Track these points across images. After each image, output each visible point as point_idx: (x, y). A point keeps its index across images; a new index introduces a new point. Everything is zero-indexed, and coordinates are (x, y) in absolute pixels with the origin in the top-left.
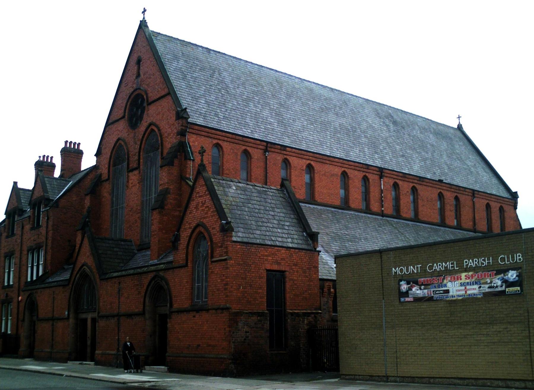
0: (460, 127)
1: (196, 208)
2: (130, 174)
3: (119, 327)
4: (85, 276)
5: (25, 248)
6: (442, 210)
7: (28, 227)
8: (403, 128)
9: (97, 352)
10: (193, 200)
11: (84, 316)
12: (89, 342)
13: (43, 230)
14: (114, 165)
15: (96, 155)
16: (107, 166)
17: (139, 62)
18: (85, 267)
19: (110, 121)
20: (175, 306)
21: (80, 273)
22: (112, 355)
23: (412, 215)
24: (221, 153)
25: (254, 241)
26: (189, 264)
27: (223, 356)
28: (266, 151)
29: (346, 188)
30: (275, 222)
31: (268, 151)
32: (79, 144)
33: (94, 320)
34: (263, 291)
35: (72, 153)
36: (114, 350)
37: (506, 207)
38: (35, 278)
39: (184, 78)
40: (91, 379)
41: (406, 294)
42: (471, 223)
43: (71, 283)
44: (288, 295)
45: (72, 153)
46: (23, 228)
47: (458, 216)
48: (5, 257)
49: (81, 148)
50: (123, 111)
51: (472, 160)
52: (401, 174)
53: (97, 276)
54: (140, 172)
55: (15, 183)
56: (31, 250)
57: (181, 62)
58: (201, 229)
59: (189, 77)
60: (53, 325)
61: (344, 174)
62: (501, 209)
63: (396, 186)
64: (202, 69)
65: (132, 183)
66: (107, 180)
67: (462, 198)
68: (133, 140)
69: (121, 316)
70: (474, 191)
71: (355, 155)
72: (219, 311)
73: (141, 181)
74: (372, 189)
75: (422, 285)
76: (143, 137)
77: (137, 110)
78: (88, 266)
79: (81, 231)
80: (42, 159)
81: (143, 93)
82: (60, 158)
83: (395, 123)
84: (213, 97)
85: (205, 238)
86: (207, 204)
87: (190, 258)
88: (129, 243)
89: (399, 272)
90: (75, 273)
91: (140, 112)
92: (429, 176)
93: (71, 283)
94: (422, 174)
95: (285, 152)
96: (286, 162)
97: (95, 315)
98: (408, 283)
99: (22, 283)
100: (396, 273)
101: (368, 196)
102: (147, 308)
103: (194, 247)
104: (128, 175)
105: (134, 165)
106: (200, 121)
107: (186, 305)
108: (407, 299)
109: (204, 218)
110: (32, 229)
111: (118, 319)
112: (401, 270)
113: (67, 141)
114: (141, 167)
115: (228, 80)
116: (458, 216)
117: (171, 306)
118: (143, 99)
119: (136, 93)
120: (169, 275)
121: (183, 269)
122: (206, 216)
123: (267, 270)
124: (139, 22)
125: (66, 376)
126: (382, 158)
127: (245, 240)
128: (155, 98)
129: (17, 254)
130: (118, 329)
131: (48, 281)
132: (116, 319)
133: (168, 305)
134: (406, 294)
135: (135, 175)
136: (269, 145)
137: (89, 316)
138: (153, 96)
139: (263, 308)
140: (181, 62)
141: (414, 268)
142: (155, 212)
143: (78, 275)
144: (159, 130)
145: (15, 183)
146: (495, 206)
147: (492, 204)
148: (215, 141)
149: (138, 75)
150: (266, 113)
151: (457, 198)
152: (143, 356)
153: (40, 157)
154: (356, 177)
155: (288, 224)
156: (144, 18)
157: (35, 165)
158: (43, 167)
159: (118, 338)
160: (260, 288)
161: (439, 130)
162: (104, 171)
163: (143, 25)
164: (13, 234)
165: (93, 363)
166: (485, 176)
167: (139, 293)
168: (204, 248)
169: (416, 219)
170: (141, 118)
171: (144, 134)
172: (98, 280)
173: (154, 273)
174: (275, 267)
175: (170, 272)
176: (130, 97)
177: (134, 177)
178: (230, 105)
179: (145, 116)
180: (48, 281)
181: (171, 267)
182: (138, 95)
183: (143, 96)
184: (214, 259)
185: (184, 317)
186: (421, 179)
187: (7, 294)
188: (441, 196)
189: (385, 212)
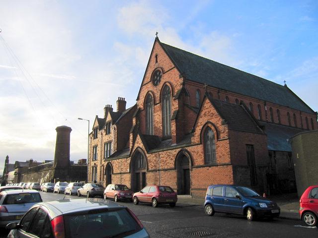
0: (286, 85)
7: (104, 134)
11: (138, 172)
15: (137, 100)
17: (156, 56)
19: (145, 83)
35: (122, 103)
42: (301, 126)
45: (122, 103)
48: (93, 148)
49: (125, 100)
55: (97, 116)
63: (271, 109)
68: (157, 91)
70: (301, 111)
81: (160, 70)
83: (262, 83)
85: (211, 129)
87: (202, 140)
91: (158, 78)
103: (204, 134)
107: (202, 164)
118: (160, 72)
123: (247, 145)
136: (220, 90)
139: (246, 164)
145: (97, 116)
148: (197, 88)
149: (157, 62)
151: (278, 111)
158: (108, 109)
162: (141, 106)
163: (157, 40)
174: (249, 143)
178: (199, 73)
179: (162, 79)
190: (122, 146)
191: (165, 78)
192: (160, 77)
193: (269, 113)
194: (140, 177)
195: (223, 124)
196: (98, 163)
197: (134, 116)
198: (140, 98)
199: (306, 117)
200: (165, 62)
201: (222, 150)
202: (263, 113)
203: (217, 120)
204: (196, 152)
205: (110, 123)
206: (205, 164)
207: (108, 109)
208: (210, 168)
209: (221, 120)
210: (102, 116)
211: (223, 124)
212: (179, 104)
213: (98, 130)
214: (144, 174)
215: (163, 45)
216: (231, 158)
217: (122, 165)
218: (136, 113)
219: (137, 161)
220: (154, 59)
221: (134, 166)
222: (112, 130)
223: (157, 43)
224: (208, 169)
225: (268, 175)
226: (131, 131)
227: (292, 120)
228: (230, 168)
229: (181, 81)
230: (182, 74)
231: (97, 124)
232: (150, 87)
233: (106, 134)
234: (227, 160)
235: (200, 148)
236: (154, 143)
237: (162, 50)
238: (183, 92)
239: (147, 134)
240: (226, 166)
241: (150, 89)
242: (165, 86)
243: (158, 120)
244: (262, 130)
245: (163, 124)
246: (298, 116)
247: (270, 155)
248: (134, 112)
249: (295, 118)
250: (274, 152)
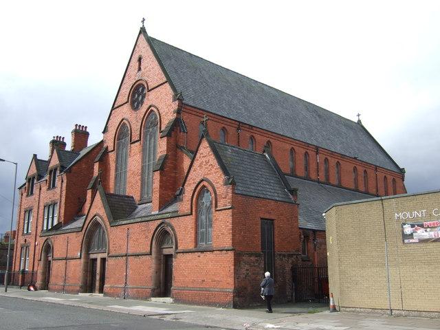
0: (359, 121)
1: (200, 166)
2: (132, 145)
4: (96, 225)
5: (42, 205)
6: (356, 180)
7: (25, 194)
8: (325, 120)
9: (105, 286)
10: (198, 160)
11: (93, 256)
12: (98, 277)
13: (58, 190)
14: (119, 139)
15: (104, 132)
16: (113, 141)
17: (140, 60)
18: (97, 217)
19: (116, 106)
20: (180, 248)
23: (336, 182)
25: (251, 194)
26: (194, 213)
28: (238, 129)
29: (293, 160)
30: (264, 179)
31: (240, 129)
33: (103, 260)
34: (258, 236)
35: (81, 135)
37: (397, 180)
39: (176, 72)
41: (411, 236)
42: (375, 190)
43: (84, 229)
44: (276, 239)
45: (81, 135)
46: (40, 189)
47: (366, 184)
50: (127, 97)
51: (370, 146)
52: (330, 152)
55: (35, 156)
56: (48, 206)
57: (173, 61)
58: (205, 183)
59: (179, 72)
61: (292, 150)
62: (394, 180)
63: (326, 160)
64: (188, 67)
66: (112, 151)
67: (369, 171)
68: (134, 119)
70: (376, 166)
71: (298, 136)
72: (224, 252)
73: (144, 150)
74: (311, 162)
75: (428, 227)
76: (144, 116)
77: (138, 96)
78: (99, 216)
79: (90, 190)
83: (319, 116)
84: (198, 87)
85: (208, 191)
86: (211, 162)
88: (131, 199)
89: (401, 217)
91: (140, 98)
92: (347, 154)
93: (84, 229)
94: (343, 153)
95: (252, 131)
96: (252, 138)
97: (105, 255)
98: (413, 226)
99: (40, 228)
100: (399, 217)
102: (154, 250)
105: (135, 138)
106: (191, 103)
107: (191, 247)
108: (411, 241)
109: (208, 174)
110: (49, 189)
111: (127, 259)
112: (405, 215)
115: (207, 77)
116: (366, 184)
117: (177, 248)
119: (137, 83)
120: (174, 222)
123: (261, 219)
126: (316, 140)
127: (244, 193)
128: (155, 86)
129: (35, 209)
132: (124, 258)
133: (174, 247)
134: (411, 236)
137: (99, 257)
138: (151, 85)
139: (259, 250)
140: (173, 61)
141: (419, 213)
145: (35, 156)
146: (390, 178)
147: (388, 177)
150: (235, 102)
151: (365, 171)
154: (300, 151)
155: (272, 181)
158: (57, 144)
160: (256, 233)
161: (346, 123)
163: (143, 31)
164: (32, 193)
166: (381, 157)
167: (147, 237)
168: (207, 199)
169: (340, 186)
170: (142, 102)
171: (145, 114)
172: (108, 227)
173: (161, 220)
174: (267, 216)
175: (176, 219)
176: (133, 86)
177: (136, 148)
179: (145, 100)
182: (139, 85)
183: (143, 85)
185: (189, 256)
186: (343, 156)
188: (355, 169)
189: (320, 180)
190: (75, 208)
191: (151, 99)
192: (144, 97)
193: (322, 168)
194: (96, 267)
195: (226, 184)
196: (31, 240)
197: (97, 160)
198: (110, 129)
199: (385, 177)
200: (152, 72)
201: (222, 227)
202: (313, 166)
203: (217, 177)
204: (184, 230)
205: (56, 169)
206: (196, 247)
207: (57, 144)
208: (202, 255)
209: (223, 176)
210: (44, 155)
211: (226, 184)
212: (168, 143)
213: (58, 172)
214: (103, 260)
215: (151, 42)
216: (233, 239)
217: (69, 244)
218: (100, 155)
219: (93, 234)
220: (135, 63)
221: (88, 245)
222: (58, 183)
223: (142, 36)
224: (199, 256)
225: (293, 270)
226: (90, 186)
227: (361, 180)
228: (231, 255)
229: (175, 105)
230: (178, 97)
231: (34, 171)
232: (126, 112)
233: (49, 189)
234: (227, 242)
235: (190, 221)
236: (121, 208)
237: (148, 48)
238: (176, 125)
239: (122, 194)
241: (125, 116)
242: (150, 112)
243: (134, 172)
244: (291, 197)
245: (142, 178)
246: (371, 173)
247: (307, 237)
248: (98, 153)
249: (366, 177)
250: (314, 231)
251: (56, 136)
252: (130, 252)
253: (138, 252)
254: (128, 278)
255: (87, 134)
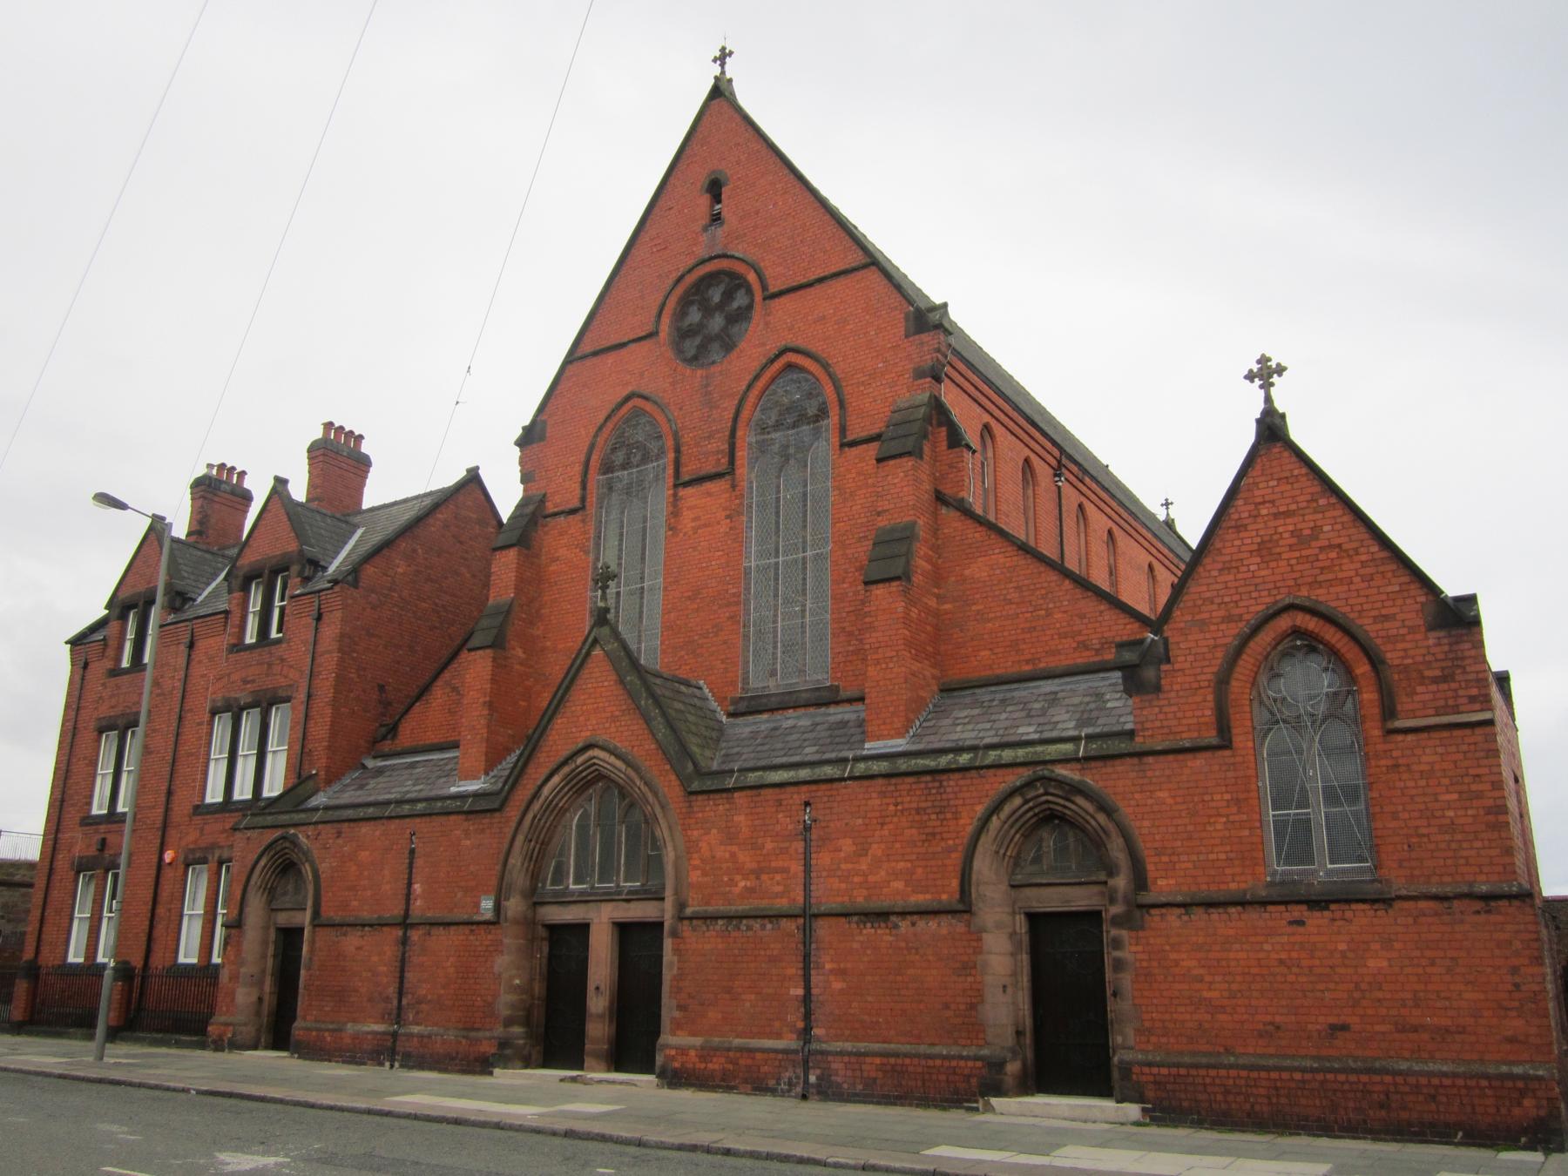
1: (1265, 550)
3: (806, 958)
15: (522, 443)
19: (579, 354)
21: (566, 770)
22: (776, 1051)
24: (990, 454)
27: (1518, 1070)
32: (361, 437)
35: (339, 458)
36: (779, 1036)
38: (243, 792)
40: (388, 1114)
45: (339, 458)
49: (247, 484)
53: (669, 786)
54: (734, 487)
60: (404, 941)
65: (694, 520)
69: (816, 916)
80: (214, 472)
82: (306, 476)
90: (536, 773)
101: (662, 731)
104: (675, 495)
113: (331, 424)
114: (742, 471)
117: (1140, 881)
121: (1208, 754)
122: (1331, 576)
124: (712, 82)
125: (199, 1092)
130: (806, 958)
131: (315, 801)
132: (790, 926)
135: (709, 494)
137: (601, 922)
142: (879, 591)
143: (556, 779)
144: (825, 366)
152: (976, 1058)
153: (210, 466)
156: (723, 72)
157: (309, 451)
158: (217, 492)
159: (807, 998)
163: (720, 92)
165: (651, 1078)
171: (757, 378)
180: (315, 801)
181: (1114, 749)
184: (1399, 724)
187: (104, 842)
224: (1300, 923)
240: (1479, 905)
251: (217, 462)
252: (828, 893)
253: (882, 903)
254: (818, 1014)
255: (362, 464)
